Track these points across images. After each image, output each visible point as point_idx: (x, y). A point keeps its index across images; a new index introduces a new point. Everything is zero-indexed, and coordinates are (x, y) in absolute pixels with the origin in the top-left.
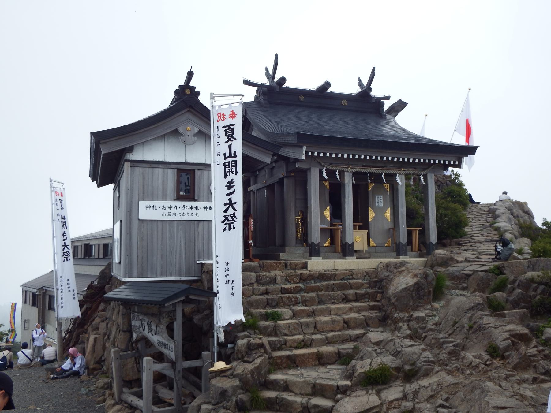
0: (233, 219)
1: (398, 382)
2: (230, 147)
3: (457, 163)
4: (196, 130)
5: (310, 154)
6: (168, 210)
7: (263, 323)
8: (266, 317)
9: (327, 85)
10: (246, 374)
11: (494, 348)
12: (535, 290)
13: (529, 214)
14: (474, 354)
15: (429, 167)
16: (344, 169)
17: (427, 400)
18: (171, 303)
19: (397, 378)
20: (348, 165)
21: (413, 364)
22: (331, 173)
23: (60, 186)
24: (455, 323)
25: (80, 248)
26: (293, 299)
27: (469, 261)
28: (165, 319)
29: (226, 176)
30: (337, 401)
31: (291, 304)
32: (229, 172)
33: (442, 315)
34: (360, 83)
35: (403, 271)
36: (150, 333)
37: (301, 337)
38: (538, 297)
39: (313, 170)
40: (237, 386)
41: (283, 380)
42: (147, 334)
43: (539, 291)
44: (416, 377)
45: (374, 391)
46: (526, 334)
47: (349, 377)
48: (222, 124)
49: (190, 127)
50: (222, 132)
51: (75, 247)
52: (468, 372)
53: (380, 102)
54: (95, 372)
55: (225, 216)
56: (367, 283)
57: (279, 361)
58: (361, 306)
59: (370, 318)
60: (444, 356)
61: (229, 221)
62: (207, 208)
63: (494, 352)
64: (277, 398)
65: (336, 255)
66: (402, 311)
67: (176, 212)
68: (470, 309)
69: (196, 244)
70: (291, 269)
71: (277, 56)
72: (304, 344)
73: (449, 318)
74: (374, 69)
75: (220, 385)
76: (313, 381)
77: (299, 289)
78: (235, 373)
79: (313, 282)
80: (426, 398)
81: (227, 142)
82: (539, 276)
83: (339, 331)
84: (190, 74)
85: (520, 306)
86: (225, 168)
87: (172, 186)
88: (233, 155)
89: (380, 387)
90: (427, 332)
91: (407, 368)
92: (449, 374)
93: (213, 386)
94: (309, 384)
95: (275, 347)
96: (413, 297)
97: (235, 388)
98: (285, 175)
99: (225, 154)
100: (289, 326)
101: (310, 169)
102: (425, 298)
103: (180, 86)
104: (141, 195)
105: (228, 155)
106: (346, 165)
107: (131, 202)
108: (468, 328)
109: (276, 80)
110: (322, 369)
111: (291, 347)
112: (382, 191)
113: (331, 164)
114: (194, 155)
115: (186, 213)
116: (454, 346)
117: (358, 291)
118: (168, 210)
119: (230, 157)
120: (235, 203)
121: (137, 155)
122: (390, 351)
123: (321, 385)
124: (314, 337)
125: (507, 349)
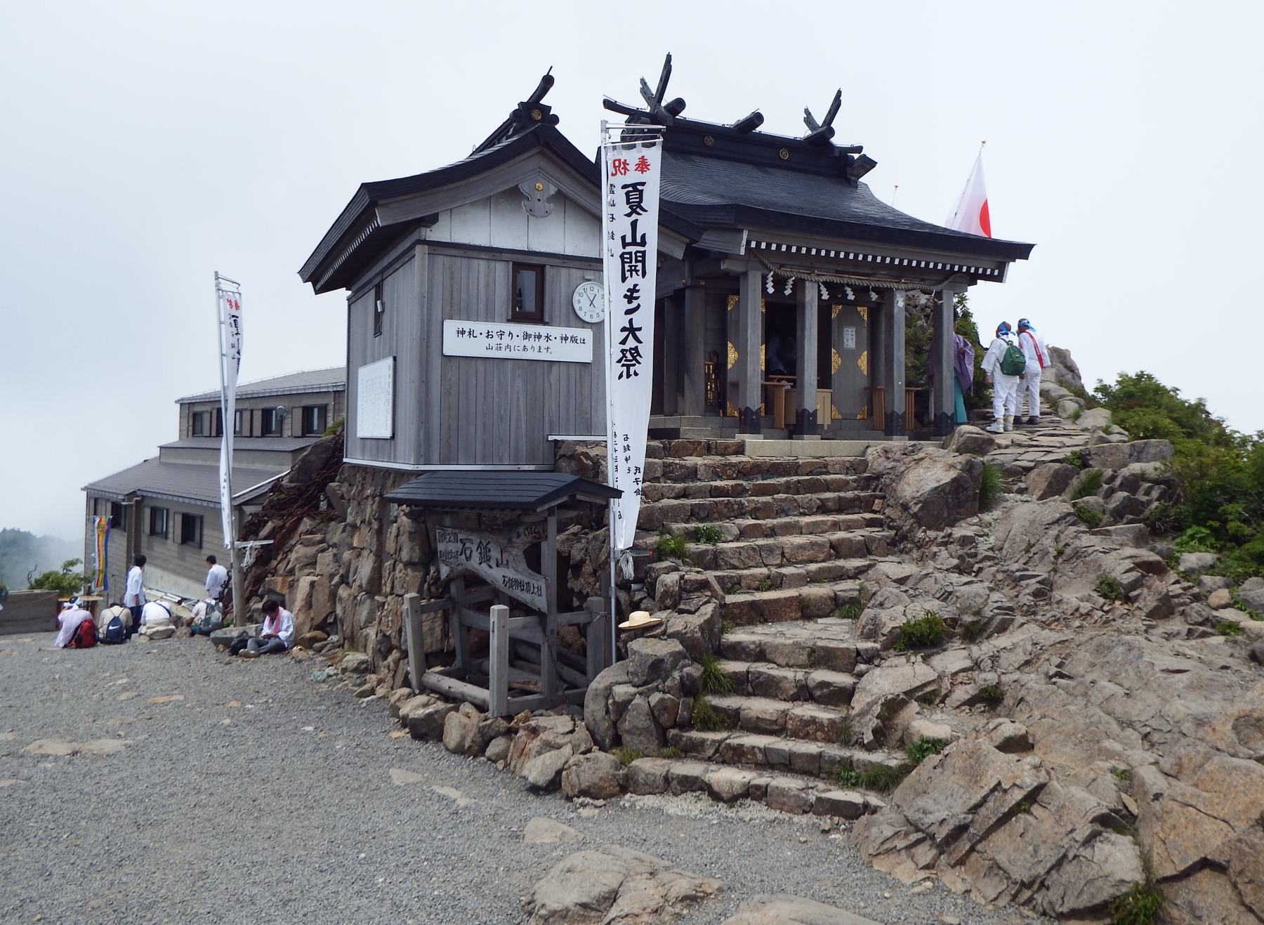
0: (634, 358)
1: (957, 643)
2: (634, 225)
3: (996, 273)
4: (553, 190)
5: (753, 245)
6: (496, 340)
7: (692, 546)
8: (695, 536)
9: (757, 118)
10: (693, 631)
11: (1109, 585)
12: (1147, 493)
13: (1072, 371)
14: (1079, 595)
15: (946, 279)
16: (806, 277)
17: (1018, 669)
18: (546, 507)
19: (951, 636)
20: (811, 270)
21: (978, 613)
22: (780, 283)
23: (233, 288)
24: (1031, 546)
25: (206, 417)
27: (1020, 445)
28: (523, 537)
29: (624, 279)
30: (860, 675)
32: (631, 271)
33: (1001, 535)
34: (809, 120)
35: (922, 459)
36: (484, 565)
37: (764, 571)
38: (1156, 504)
39: (751, 274)
40: (680, 653)
41: (754, 643)
42: (477, 566)
43: (1155, 494)
44: (985, 635)
45: (919, 658)
46: (1159, 562)
47: (870, 635)
48: (620, 180)
49: (542, 183)
50: (620, 195)
51: (195, 415)
52: (1077, 623)
54: (317, 645)
55: (622, 351)
56: (854, 481)
57: (736, 611)
58: (851, 520)
59: (873, 540)
60: (1026, 599)
61: (630, 358)
62: (566, 339)
63: (1109, 589)
64: (748, 672)
65: (776, 432)
66: (929, 528)
67: (512, 343)
68: (1053, 523)
69: (547, 405)
70: (717, 454)
71: (669, 58)
72: (775, 582)
73: (1018, 539)
74: (839, 93)
75: (649, 651)
76: (810, 644)
77: (740, 489)
78: (669, 631)
79: (759, 477)
80: (1017, 665)
81: (629, 215)
82: (1156, 469)
83: (823, 561)
84: (548, 82)
85: (1125, 520)
86: (623, 263)
87: (505, 293)
88: (639, 240)
89: (928, 652)
90: (981, 562)
91: (968, 619)
92: (1043, 628)
93: (635, 653)
94: (803, 648)
95: (733, 586)
96: (947, 503)
97: (677, 657)
98: (689, 284)
99: (623, 238)
100: (739, 551)
101: (745, 274)
102: (968, 505)
103: (521, 104)
104: (448, 309)
105: (629, 240)
106: (808, 268)
107: (429, 320)
108: (1055, 553)
109: (664, 104)
110: (810, 625)
111: (749, 588)
112: (854, 320)
113: (782, 266)
114: (554, 236)
115: (529, 347)
116: (1039, 582)
117: (842, 494)
118: (496, 340)
119: (634, 243)
120: (640, 329)
121: (438, 233)
122: (933, 592)
123: (825, 649)
124: (784, 570)
125: (1136, 584)
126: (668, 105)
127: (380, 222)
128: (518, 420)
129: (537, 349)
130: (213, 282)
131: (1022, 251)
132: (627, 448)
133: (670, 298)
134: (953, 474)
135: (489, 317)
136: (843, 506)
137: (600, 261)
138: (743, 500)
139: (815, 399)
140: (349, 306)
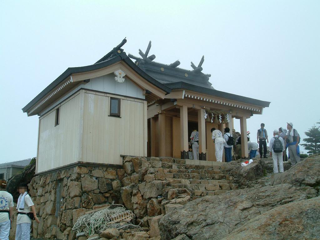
9: (178, 63)
26: (187, 176)
31: (186, 178)
34: (193, 66)
53: (207, 77)
84: (125, 41)
109: (148, 57)
127: (72, 81)
131: (266, 104)
133: (153, 118)
140: (40, 120)
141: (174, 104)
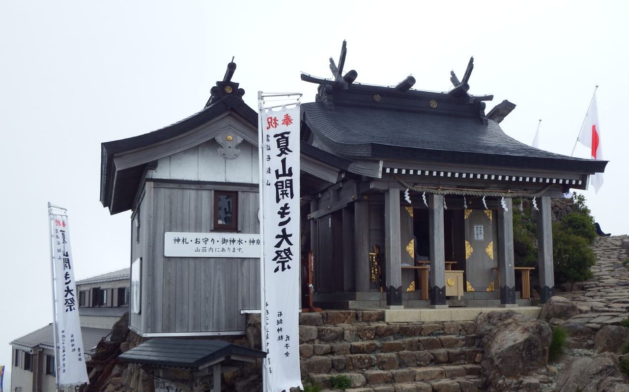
2: (284, 161)
3: (580, 183)
4: (240, 140)
5: (388, 171)
6: (202, 244)
9: (411, 81)
15: (544, 189)
16: (434, 191)
18: (207, 365)
22: (416, 196)
23: (62, 212)
26: (367, 361)
27: (596, 311)
28: (199, 386)
29: (278, 200)
32: (283, 194)
33: (560, 382)
34: (454, 79)
35: (510, 324)
39: (392, 191)
48: (273, 131)
50: (273, 142)
55: (277, 252)
56: (463, 340)
58: (454, 370)
61: (282, 258)
65: (423, 302)
66: (508, 376)
67: (214, 247)
69: (240, 289)
70: (363, 321)
71: (345, 44)
73: (570, 386)
77: (373, 347)
79: (392, 337)
81: (279, 155)
84: (232, 67)
86: (277, 189)
87: (208, 212)
88: (287, 172)
96: (522, 358)
99: (277, 171)
101: (388, 191)
102: (539, 359)
103: (218, 83)
104: (168, 224)
105: (281, 172)
107: (155, 233)
109: (343, 74)
113: (415, 184)
114: (236, 172)
115: (226, 249)
117: (451, 350)
118: (202, 244)
119: (284, 175)
120: (291, 235)
121: (162, 173)
126: (347, 75)
128: (219, 300)
129: (232, 250)
130: (47, 209)
132: (72, 341)
134: (526, 336)
135: (198, 228)
136: (451, 359)
137: (257, 186)
138: (372, 356)
139: (451, 282)
141: (371, 187)
